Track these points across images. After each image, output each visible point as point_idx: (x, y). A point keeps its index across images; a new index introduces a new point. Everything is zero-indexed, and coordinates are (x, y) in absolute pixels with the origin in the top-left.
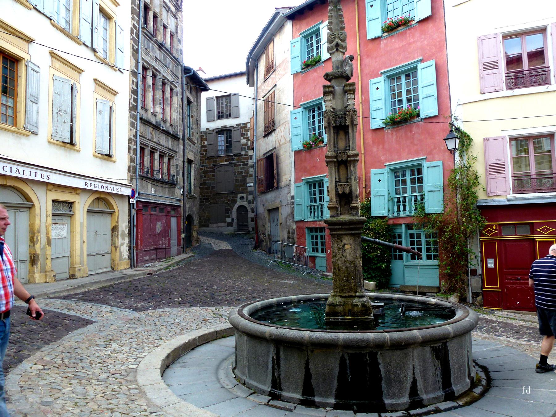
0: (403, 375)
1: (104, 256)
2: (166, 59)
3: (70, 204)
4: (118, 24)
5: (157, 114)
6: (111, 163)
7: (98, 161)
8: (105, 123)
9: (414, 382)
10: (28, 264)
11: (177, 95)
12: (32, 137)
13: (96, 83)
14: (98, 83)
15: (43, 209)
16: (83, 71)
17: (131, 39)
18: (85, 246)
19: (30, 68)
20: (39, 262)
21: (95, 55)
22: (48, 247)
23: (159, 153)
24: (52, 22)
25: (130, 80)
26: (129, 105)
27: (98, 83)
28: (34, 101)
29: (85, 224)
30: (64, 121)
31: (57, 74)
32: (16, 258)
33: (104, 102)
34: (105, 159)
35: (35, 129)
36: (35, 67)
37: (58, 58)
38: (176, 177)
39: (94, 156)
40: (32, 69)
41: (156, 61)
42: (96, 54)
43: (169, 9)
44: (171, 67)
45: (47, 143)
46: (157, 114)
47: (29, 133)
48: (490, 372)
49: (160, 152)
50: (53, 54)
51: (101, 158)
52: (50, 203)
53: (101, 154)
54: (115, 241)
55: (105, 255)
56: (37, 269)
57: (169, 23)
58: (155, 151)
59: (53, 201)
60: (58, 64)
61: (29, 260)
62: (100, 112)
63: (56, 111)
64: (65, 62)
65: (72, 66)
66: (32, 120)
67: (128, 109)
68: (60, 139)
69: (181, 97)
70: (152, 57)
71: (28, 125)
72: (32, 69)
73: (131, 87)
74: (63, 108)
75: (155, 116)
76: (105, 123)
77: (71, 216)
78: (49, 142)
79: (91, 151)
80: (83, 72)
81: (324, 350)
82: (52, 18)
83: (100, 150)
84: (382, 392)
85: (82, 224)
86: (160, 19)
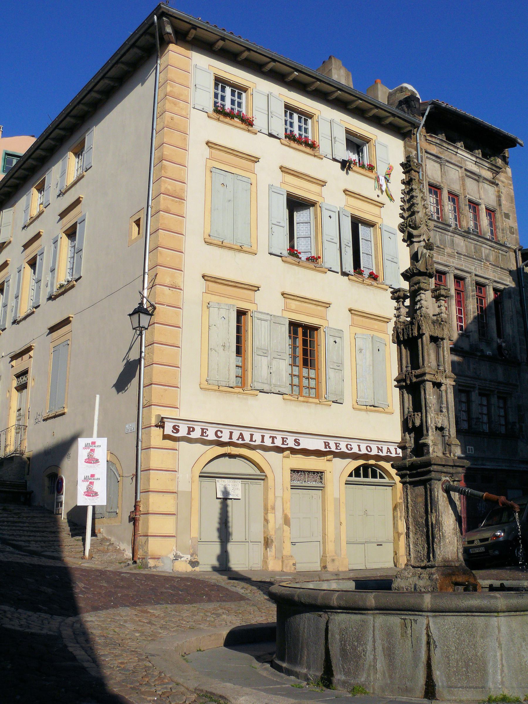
0: (361, 648)
1: (381, 545)
2: (480, 250)
3: (319, 474)
4: (384, 228)
5: (471, 334)
10: (262, 546)
11: (510, 297)
14: (209, 279)
15: (279, 481)
16: (257, 289)
18: (343, 528)
19: (256, 318)
22: (286, 527)
23: (477, 392)
27: (209, 279)
28: (262, 354)
29: (343, 500)
32: (247, 538)
33: (365, 337)
34: (371, 411)
36: (263, 315)
38: (518, 426)
40: (258, 319)
41: (459, 258)
43: (479, 176)
44: (492, 258)
46: (471, 334)
49: (479, 389)
52: (288, 473)
54: (397, 524)
55: (383, 544)
56: (271, 552)
57: (483, 197)
58: (472, 390)
59: (293, 471)
61: (263, 542)
62: (361, 350)
64: (317, 303)
65: (314, 302)
69: (518, 298)
70: (449, 255)
71: (255, 384)
72: (258, 319)
75: (468, 337)
77: (322, 489)
81: (289, 592)
83: (361, 400)
85: (338, 501)
86: (463, 197)
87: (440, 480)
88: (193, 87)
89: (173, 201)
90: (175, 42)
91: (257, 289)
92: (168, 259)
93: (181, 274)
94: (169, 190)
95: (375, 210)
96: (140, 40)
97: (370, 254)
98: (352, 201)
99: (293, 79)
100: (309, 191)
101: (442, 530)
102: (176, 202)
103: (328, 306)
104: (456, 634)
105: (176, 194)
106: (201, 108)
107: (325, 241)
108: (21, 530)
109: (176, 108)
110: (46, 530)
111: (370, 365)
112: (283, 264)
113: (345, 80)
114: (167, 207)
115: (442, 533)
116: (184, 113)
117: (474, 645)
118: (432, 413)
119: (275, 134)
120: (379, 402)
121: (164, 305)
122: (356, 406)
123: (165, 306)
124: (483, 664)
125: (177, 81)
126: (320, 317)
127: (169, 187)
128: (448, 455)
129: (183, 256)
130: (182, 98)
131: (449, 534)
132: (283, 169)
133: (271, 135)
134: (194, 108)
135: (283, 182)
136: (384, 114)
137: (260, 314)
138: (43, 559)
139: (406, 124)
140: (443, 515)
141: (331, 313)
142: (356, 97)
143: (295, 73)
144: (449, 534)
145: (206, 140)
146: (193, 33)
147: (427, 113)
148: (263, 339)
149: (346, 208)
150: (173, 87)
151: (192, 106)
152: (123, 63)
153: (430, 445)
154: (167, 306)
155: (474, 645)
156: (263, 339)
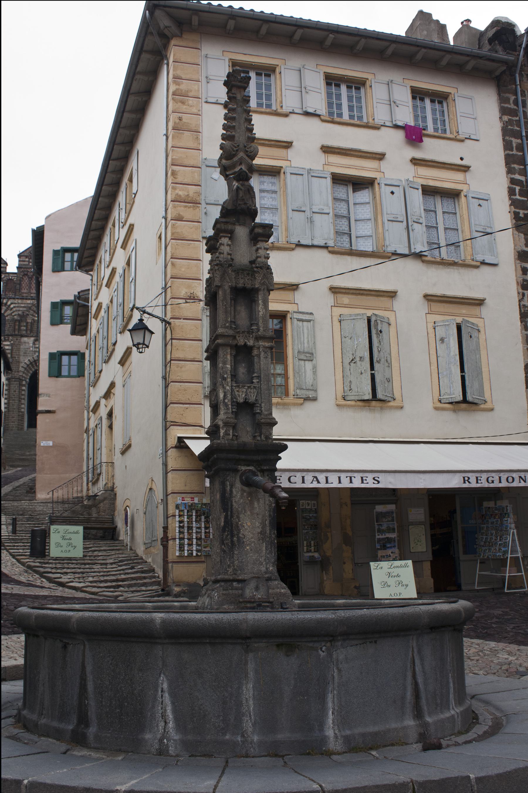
6: (480, 413)
7: (448, 416)
8: (452, 354)
9: (112, 385)
12: (309, 405)
13: (428, 300)
17: (510, 205)
20: (331, 567)
21: (423, 261)
24: (330, 249)
25: (516, 270)
26: (520, 311)
28: (305, 358)
30: (360, 371)
31: (346, 311)
33: (447, 323)
35: (311, 394)
36: (305, 315)
37: (344, 291)
39: (436, 409)
40: (299, 320)
42: (424, 258)
45: (336, 407)
47: (301, 401)
48: (226, 106)
50: (333, 290)
51: (454, 411)
53: (451, 403)
60: (346, 299)
62: (442, 340)
63: (347, 361)
64: (358, 292)
65: (373, 293)
66: (306, 383)
67: (519, 317)
68: (357, 398)
72: (299, 320)
73: (520, 280)
74: (358, 354)
76: (452, 354)
78: (337, 405)
79: (428, 404)
80: (484, 311)
82: (328, 245)
83: (445, 397)
84: (432, 577)
87: (236, 471)
88: (204, 80)
89: (186, 207)
90: (179, 34)
91: (480, 303)
92: (183, 270)
93: (200, 283)
94: (180, 196)
95: (459, 176)
96: (146, 43)
97: (435, 225)
98: (334, 159)
99: (331, 43)
100: (363, 169)
101: (238, 535)
102: (190, 207)
103: (393, 294)
104: (111, 664)
105: (189, 199)
106: (213, 100)
107: (386, 222)
108: (70, 563)
109: (185, 107)
110: (97, 562)
111: (456, 355)
112: (330, 256)
113: (438, 34)
114: (179, 214)
115: (238, 538)
116: (194, 110)
117: (131, 680)
118: (228, 385)
119: (311, 110)
120: (474, 397)
121: (180, 319)
122: (439, 405)
123: (182, 320)
124: (140, 705)
125: (184, 77)
126: (383, 309)
127: (181, 193)
128: (259, 438)
129: (202, 263)
130: (190, 94)
131: (253, 540)
132: (327, 150)
133: (307, 114)
134: (206, 102)
135: (327, 163)
136: (462, 59)
137: (301, 315)
138: (67, 590)
139: (495, 65)
140: (241, 516)
141: (398, 304)
142: (418, 46)
143: (331, 35)
144: (253, 540)
145: (320, 146)
146: (195, 20)
147: (523, 46)
148: (306, 341)
149: (416, 180)
150: (179, 85)
151: (204, 100)
152: (140, 73)
153: (221, 426)
154: (184, 319)
155: (131, 680)
156: (306, 341)
